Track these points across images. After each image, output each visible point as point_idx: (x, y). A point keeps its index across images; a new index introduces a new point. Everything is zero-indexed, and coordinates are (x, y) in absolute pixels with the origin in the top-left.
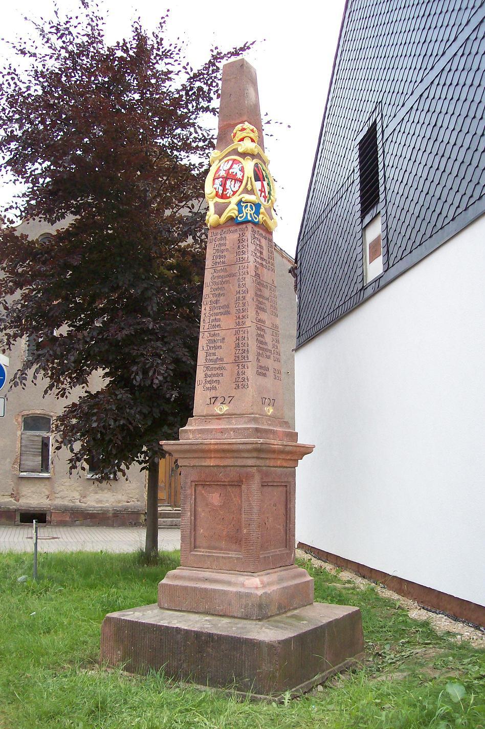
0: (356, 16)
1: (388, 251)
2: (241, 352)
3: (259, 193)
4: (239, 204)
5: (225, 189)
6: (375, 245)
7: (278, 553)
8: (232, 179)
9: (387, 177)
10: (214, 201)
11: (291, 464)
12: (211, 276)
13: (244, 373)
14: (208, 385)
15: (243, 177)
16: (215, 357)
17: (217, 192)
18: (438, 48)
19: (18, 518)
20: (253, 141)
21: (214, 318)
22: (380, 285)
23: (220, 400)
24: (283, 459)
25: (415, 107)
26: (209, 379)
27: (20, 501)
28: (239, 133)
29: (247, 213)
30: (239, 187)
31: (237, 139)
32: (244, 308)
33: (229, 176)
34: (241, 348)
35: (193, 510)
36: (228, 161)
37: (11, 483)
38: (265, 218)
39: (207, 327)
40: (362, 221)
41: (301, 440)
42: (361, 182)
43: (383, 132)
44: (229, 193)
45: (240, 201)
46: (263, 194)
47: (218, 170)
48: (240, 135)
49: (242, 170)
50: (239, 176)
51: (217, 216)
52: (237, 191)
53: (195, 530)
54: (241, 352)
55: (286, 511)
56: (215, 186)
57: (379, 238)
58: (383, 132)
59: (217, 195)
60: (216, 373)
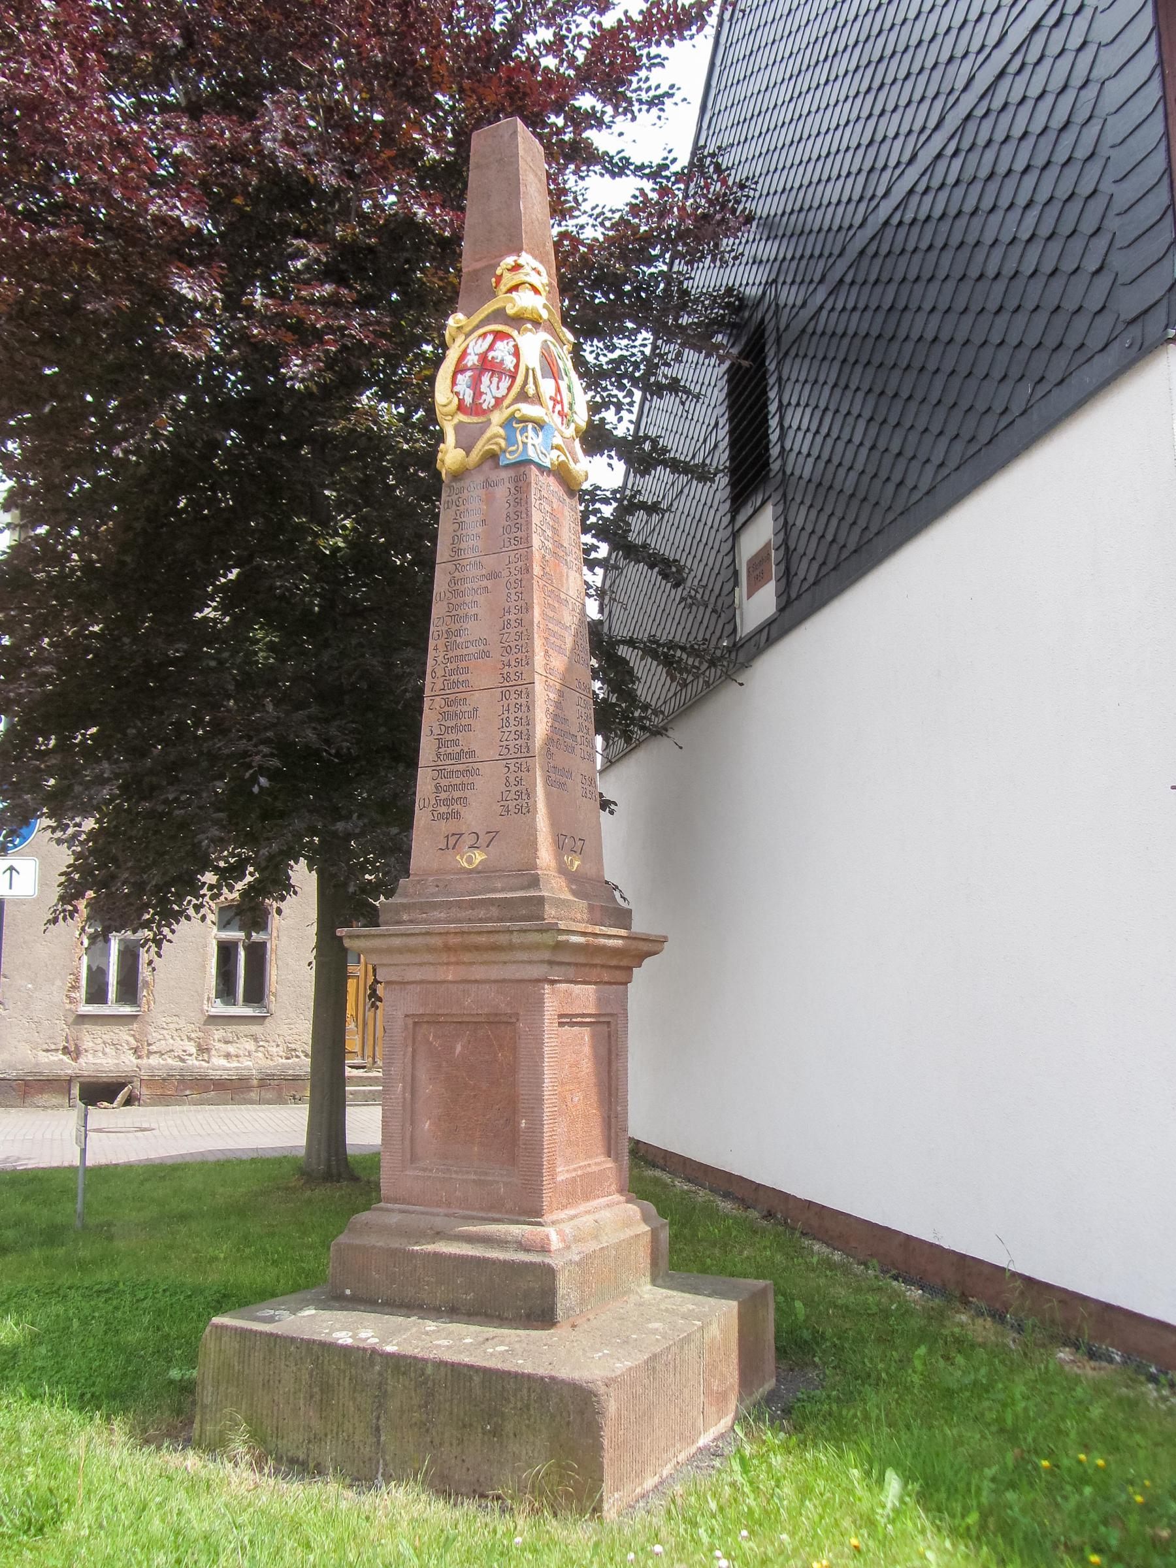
0: (725, 120)
1: (787, 569)
2: (513, 736)
3: (551, 404)
4: (508, 424)
5: (478, 394)
6: (758, 563)
7: (594, 1168)
8: (493, 372)
9: (786, 425)
10: (456, 421)
11: (619, 975)
12: (449, 577)
13: (519, 782)
14: (443, 809)
15: (517, 366)
16: (458, 749)
17: (461, 401)
18: (897, 151)
19: (76, 1091)
20: (536, 291)
21: (454, 666)
22: (773, 632)
23: (469, 840)
24: (602, 966)
25: (848, 279)
26: (443, 795)
27: (82, 1060)
28: (507, 275)
29: (525, 444)
30: (509, 389)
31: (503, 288)
32: (519, 643)
33: (487, 365)
34: (513, 729)
35: (409, 1079)
36: (484, 335)
37: (61, 1030)
38: (562, 458)
39: (439, 685)
40: (733, 520)
41: (639, 926)
42: (732, 445)
43: (778, 340)
44: (488, 401)
45: (512, 418)
46: (559, 407)
47: (464, 354)
48: (509, 280)
49: (517, 353)
50: (510, 362)
51: (460, 453)
52: (504, 397)
53: (412, 1123)
54: (513, 736)
55: (610, 1078)
56: (456, 389)
57: (768, 544)
58: (778, 340)
59: (461, 407)
60: (458, 781)
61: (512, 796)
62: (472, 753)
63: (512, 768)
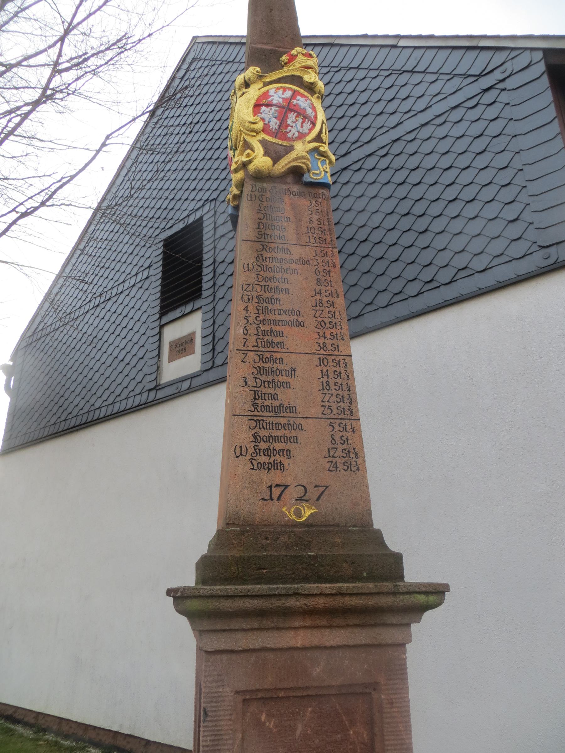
61: (339, 453)
62: (292, 409)
63: (337, 428)
